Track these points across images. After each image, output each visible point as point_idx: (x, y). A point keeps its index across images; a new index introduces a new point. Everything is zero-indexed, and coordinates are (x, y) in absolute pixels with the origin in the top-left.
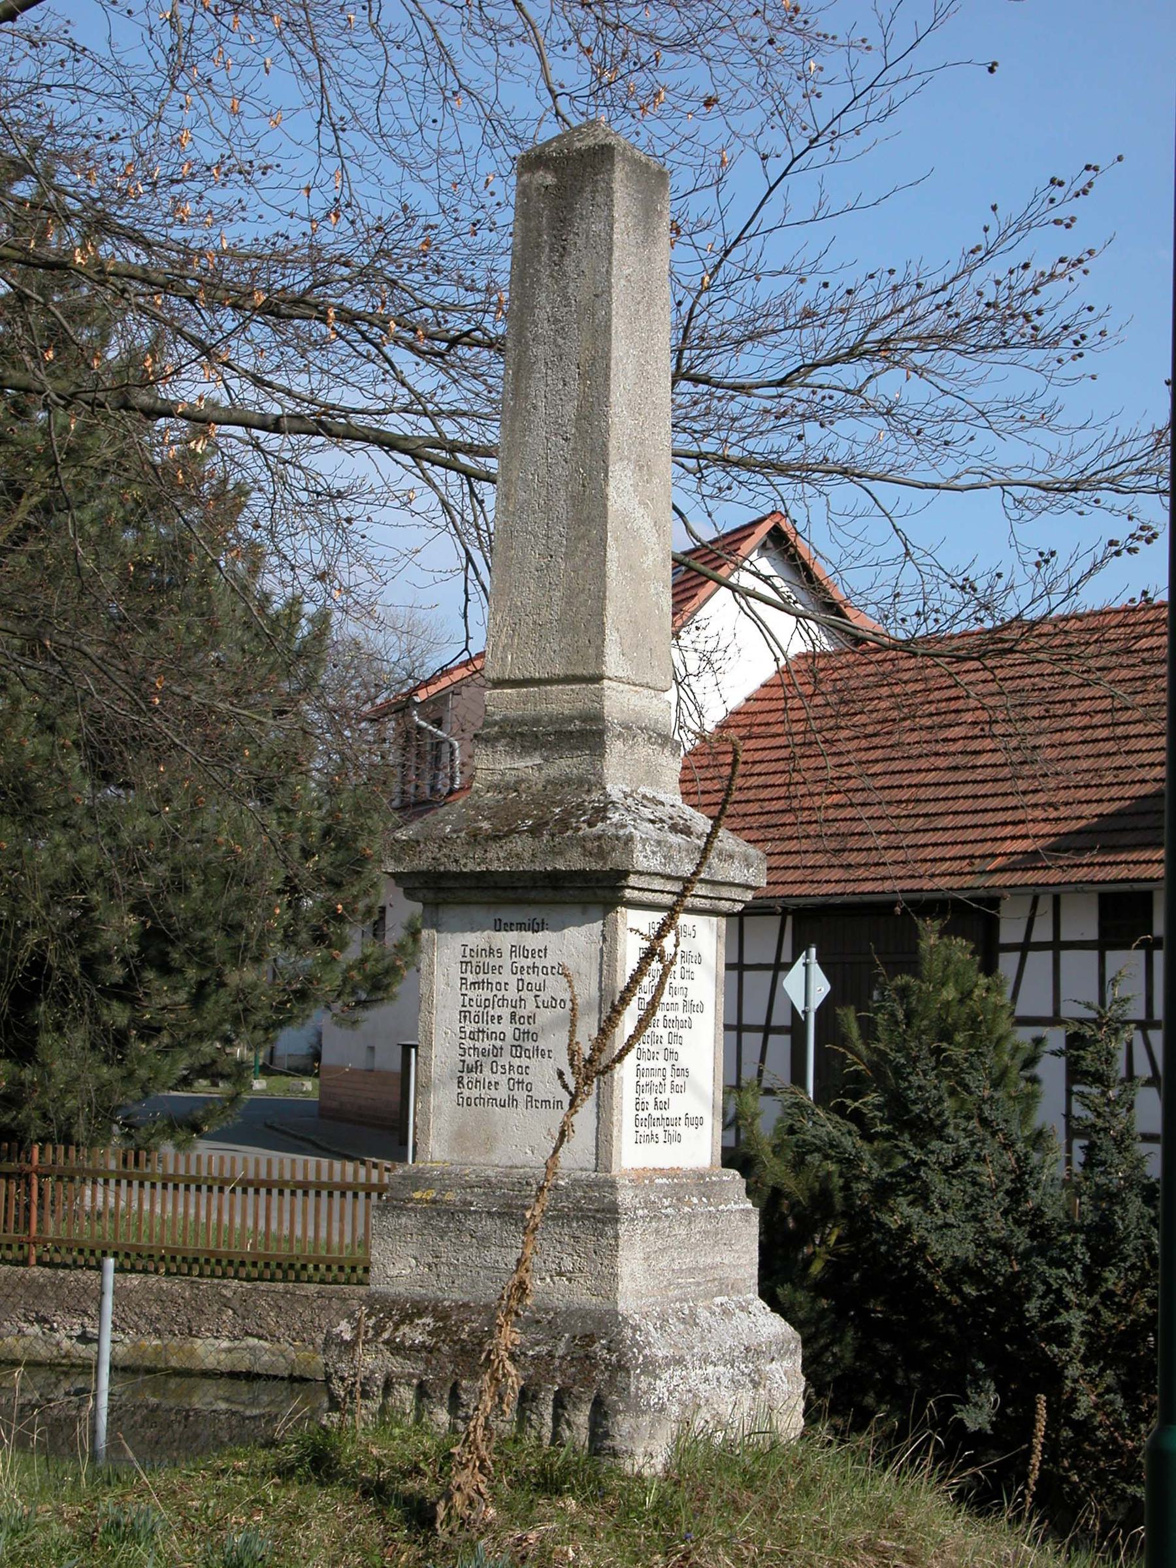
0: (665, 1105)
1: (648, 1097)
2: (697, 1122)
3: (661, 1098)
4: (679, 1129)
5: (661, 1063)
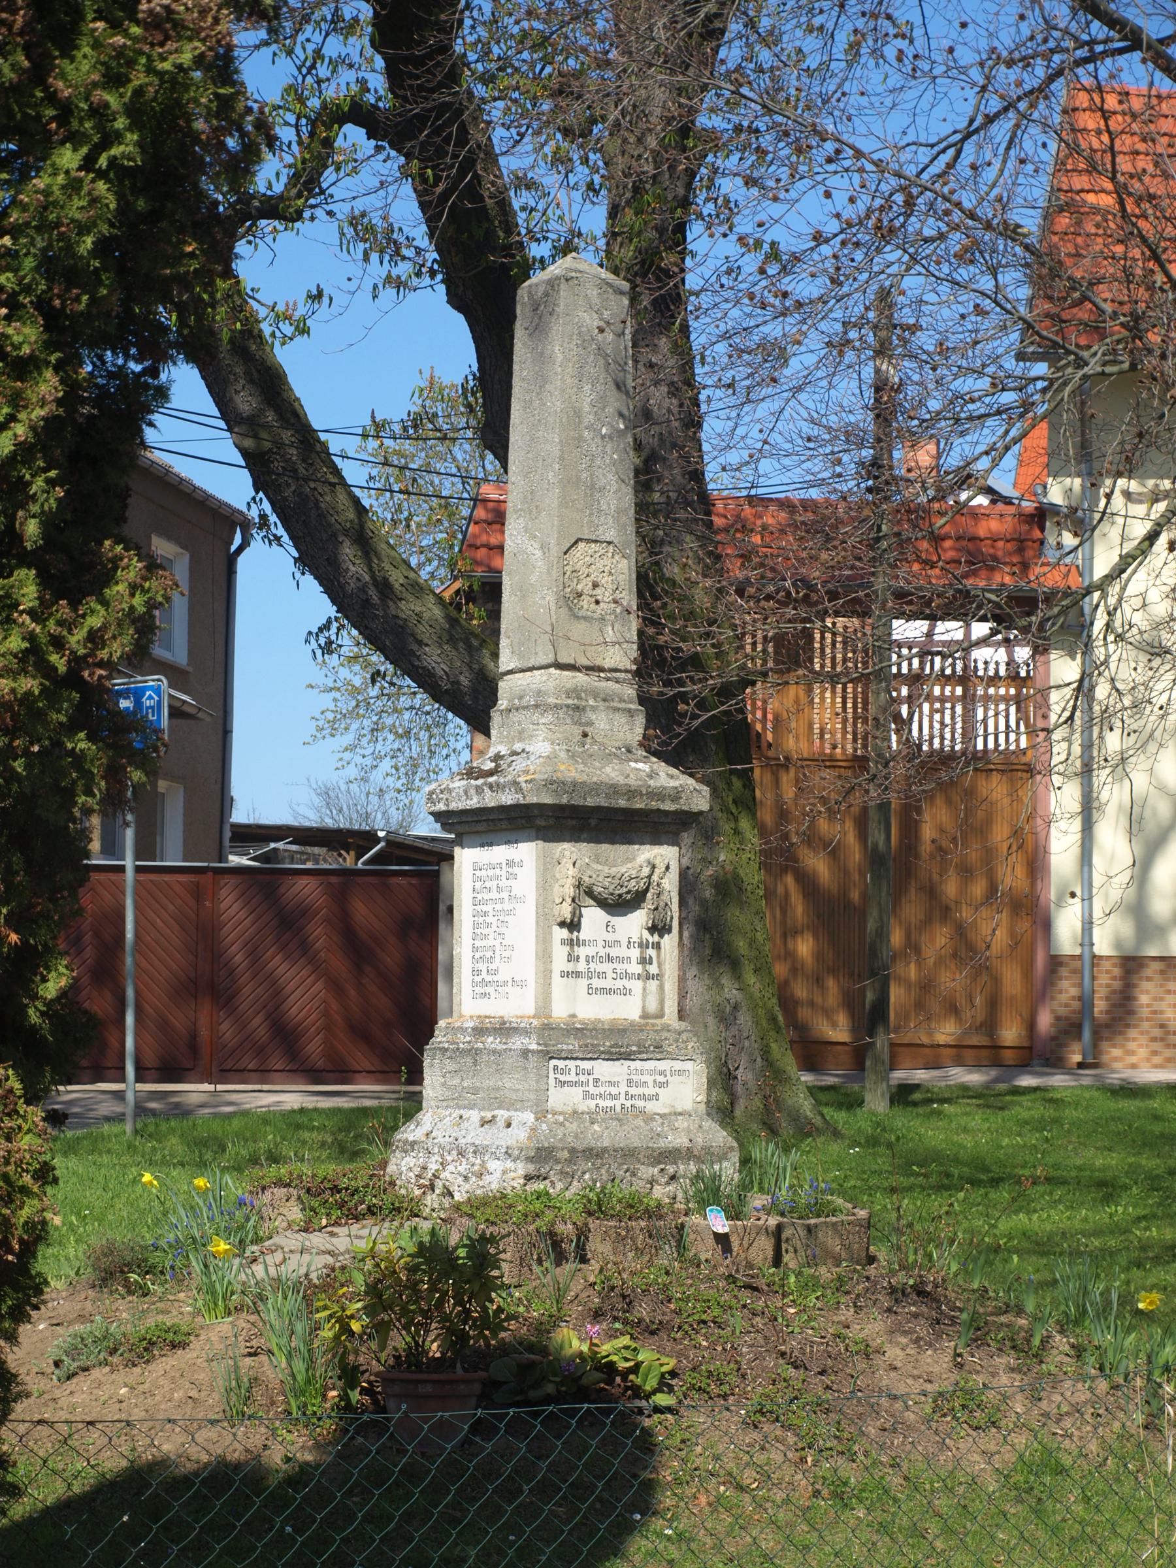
0: (496, 972)
1: (482, 967)
2: (522, 984)
3: (491, 966)
4: (506, 989)
5: (491, 942)
